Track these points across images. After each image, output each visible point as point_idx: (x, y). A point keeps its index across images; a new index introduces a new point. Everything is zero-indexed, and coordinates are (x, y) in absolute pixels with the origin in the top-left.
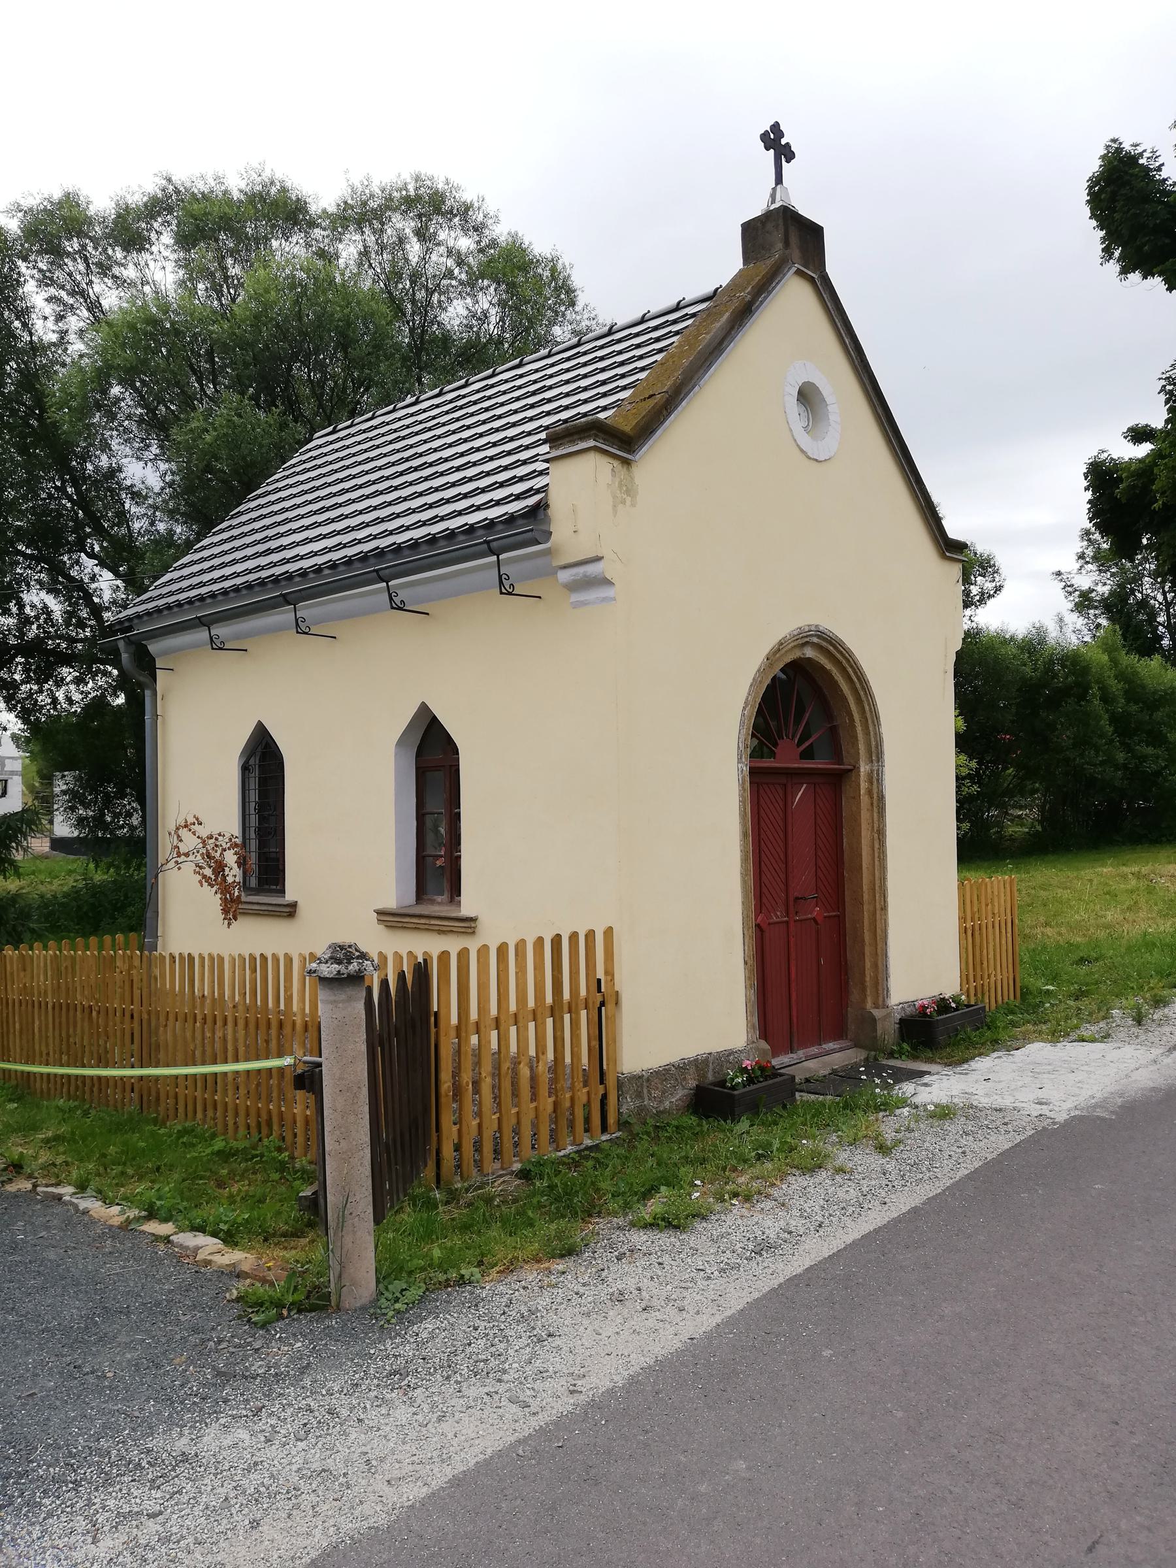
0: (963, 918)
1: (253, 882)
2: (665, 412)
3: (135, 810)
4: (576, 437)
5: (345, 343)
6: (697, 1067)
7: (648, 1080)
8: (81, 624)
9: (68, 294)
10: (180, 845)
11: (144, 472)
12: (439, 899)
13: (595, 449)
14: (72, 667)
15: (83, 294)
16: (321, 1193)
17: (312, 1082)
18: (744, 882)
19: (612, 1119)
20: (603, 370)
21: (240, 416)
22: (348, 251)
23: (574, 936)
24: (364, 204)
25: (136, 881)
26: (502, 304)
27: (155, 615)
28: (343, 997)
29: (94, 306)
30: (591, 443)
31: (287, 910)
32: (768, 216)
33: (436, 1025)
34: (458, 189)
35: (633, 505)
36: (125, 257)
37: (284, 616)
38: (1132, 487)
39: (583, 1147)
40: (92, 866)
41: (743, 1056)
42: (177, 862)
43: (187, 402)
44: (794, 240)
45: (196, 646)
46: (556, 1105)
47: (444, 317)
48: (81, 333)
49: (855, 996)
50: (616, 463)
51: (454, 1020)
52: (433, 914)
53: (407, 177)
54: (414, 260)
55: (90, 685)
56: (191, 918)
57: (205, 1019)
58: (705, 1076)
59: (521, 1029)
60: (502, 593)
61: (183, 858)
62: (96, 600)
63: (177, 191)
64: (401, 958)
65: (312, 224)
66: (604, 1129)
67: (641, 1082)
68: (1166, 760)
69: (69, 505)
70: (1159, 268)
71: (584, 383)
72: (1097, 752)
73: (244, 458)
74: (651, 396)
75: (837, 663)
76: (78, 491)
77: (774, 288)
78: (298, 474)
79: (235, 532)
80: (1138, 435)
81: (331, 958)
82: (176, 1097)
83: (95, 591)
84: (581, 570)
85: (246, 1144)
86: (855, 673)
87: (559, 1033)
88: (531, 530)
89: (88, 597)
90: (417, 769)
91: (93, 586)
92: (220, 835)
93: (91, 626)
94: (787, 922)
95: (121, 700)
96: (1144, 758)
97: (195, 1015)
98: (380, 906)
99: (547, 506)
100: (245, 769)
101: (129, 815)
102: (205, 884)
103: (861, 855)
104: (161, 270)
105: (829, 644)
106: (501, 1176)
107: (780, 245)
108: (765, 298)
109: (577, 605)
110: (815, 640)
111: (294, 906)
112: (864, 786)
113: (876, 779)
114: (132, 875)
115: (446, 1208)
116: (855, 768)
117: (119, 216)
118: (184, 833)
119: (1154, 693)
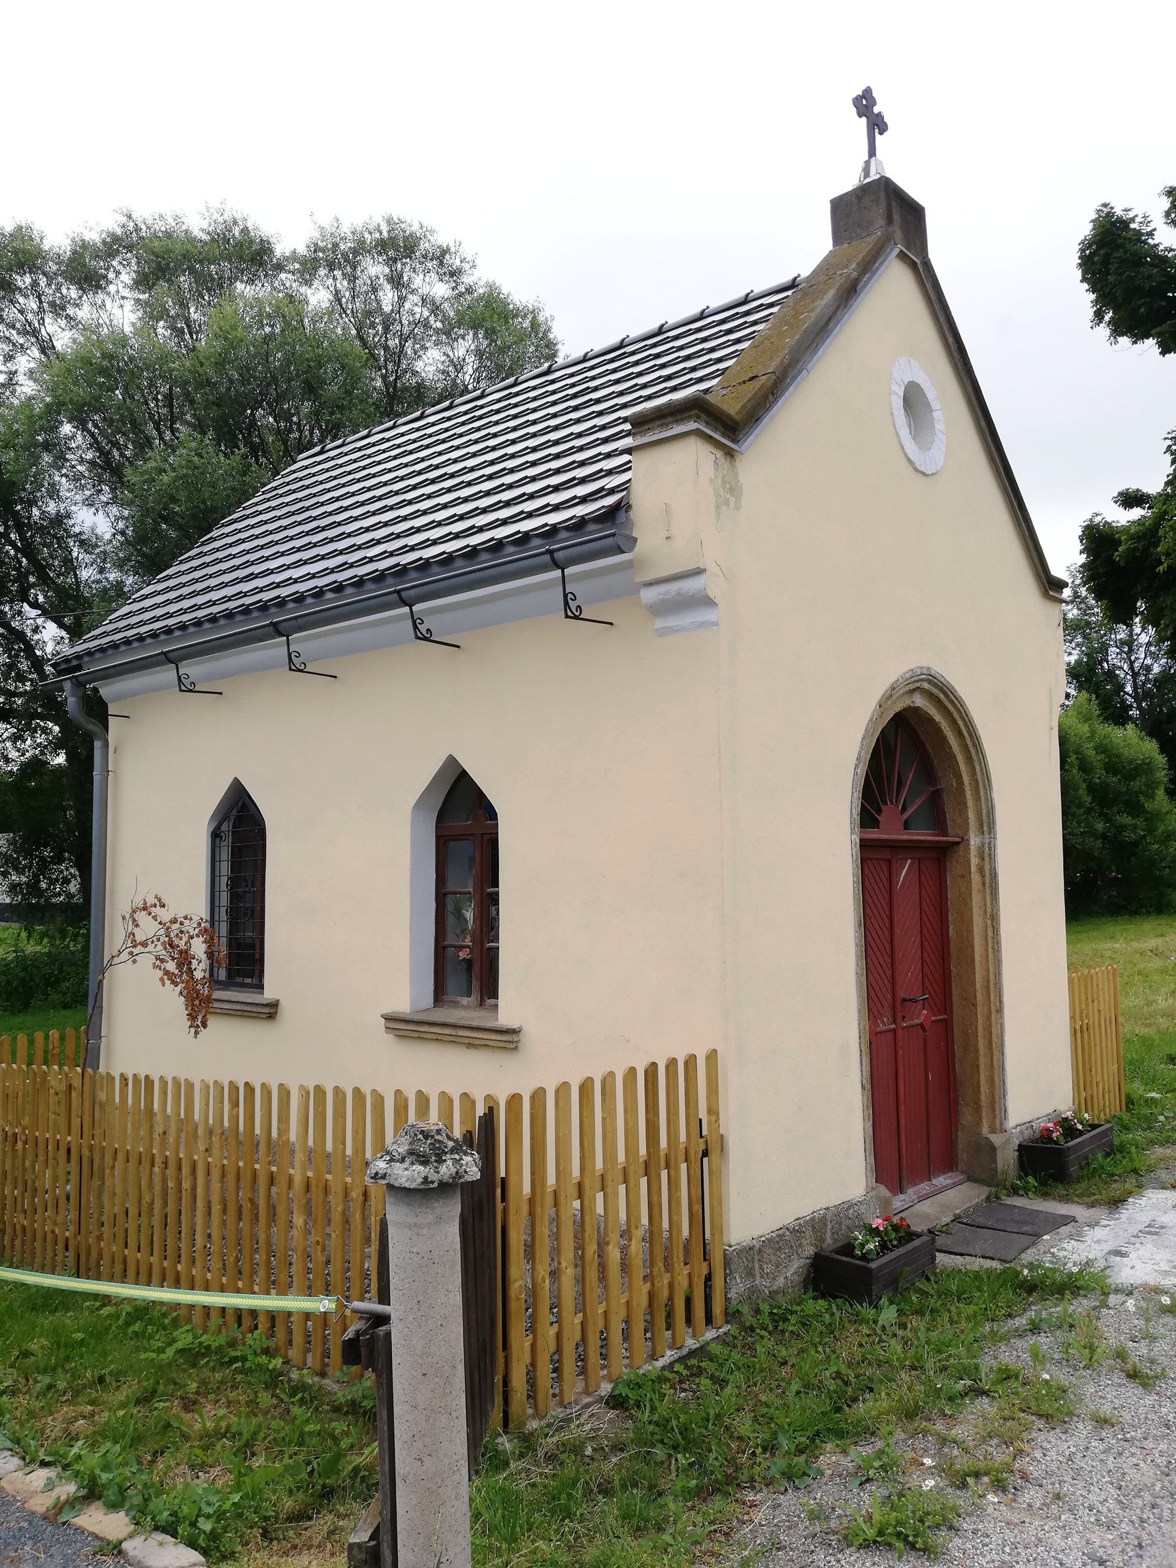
0: (1072, 1018)
1: (222, 975)
2: (771, 397)
3: (74, 876)
4: (669, 419)
5: (311, 389)
6: (813, 1227)
7: (760, 1251)
8: (21, 678)
9: (18, 333)
10: (136, 931)
11: (96, 520)
12: (465, 1001)
13: (698, 433)
14: (10, 723)
15: (35, 333)
16: (386, 1538)
17: (371, 1353)
18: (859, 982)
19: (718, 1310)
20: (578, 421)
21: (200, 456)
22: (318, 297)
23: (672, 1064)
24: (336, 245)
25: (73, 953)
26: (479, 354)
27: (110, 652)
28: (430, 1217)
29: (46, 347)
30: (692, 425)
31: (267, 1010)
32: (862, 192)
33: (503, 1200)
34: (432, 232)
35: (738, 508)
36: (80, 297)
37: (275, 649)
38: (1131, 551)
39: (685, 1351)
40: (24, 934)
41: (863, 1209)
42: (131, 953)
43: (144, 444)
44: (896, 217)
45: (157, 689)
46: (651, 1295)
47: (419, 366)
48: (31, 374)
49: (966, 1118)
50: (719, 454)
51: (527, 1188)
52: (462, 1023)
53: (378, 219)
54: (387, 308)
55: (29, 742)
56: (144, 1027)
57: (166, 1163)
58: (822, 1240)
59: (610, 1196)
60: (567, 616)
61: (139, 949)
62: (38, 653)
63: (137, 229)
64: (451, 1101)
65: (279, 267)
66: (709, 1320)
67: (754, 1254)
68: (1144, 830)
69: (12, 552)
70: (1158, 329)
71: (577, 429)
72: (1079, 822)
73: (204, 502)
74: (751, 379)
75: (947, 714)
76: (23, 538)
77: (878, 269)
78: (281, 496)
79: (207, 559)
80: (1130, 499)
81: (411, 1153)
82: (125, 1262)
83: (37, 642)
84: (674, 587)
85: (221, 1340)
86: (966, 726)
87: (655, 1198)
88: (613, 535)
89: (29, 649)
90: (438, 837)
91: (36, 637)
92: (186, 918)
93: (31, 680)
94: (894, 1031)
95: (60, 759)
96: (1123, 828)
97: (153, 1157)
98: (389, 1009)
99: (629, 507)
100: (216, 835)
101: (66, 881)
102: (168, 982)
103: (972, 946)
104: (119, 310)
105: (939, 691)
106: (587, 1406)
107: (881, 222)
108: (870, 279)
109: (663, 633)
110: (926, 685)
111: (275, 1005)
112: (974, 861)
113: (988, 854)
114: (68, 946)
115: (522, 1464)
116: (963, 841)
117: (74, 252)
118: (141, 917)
119: (1130, 762)
